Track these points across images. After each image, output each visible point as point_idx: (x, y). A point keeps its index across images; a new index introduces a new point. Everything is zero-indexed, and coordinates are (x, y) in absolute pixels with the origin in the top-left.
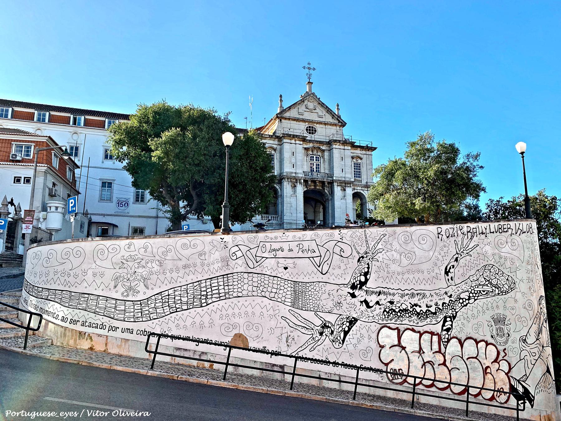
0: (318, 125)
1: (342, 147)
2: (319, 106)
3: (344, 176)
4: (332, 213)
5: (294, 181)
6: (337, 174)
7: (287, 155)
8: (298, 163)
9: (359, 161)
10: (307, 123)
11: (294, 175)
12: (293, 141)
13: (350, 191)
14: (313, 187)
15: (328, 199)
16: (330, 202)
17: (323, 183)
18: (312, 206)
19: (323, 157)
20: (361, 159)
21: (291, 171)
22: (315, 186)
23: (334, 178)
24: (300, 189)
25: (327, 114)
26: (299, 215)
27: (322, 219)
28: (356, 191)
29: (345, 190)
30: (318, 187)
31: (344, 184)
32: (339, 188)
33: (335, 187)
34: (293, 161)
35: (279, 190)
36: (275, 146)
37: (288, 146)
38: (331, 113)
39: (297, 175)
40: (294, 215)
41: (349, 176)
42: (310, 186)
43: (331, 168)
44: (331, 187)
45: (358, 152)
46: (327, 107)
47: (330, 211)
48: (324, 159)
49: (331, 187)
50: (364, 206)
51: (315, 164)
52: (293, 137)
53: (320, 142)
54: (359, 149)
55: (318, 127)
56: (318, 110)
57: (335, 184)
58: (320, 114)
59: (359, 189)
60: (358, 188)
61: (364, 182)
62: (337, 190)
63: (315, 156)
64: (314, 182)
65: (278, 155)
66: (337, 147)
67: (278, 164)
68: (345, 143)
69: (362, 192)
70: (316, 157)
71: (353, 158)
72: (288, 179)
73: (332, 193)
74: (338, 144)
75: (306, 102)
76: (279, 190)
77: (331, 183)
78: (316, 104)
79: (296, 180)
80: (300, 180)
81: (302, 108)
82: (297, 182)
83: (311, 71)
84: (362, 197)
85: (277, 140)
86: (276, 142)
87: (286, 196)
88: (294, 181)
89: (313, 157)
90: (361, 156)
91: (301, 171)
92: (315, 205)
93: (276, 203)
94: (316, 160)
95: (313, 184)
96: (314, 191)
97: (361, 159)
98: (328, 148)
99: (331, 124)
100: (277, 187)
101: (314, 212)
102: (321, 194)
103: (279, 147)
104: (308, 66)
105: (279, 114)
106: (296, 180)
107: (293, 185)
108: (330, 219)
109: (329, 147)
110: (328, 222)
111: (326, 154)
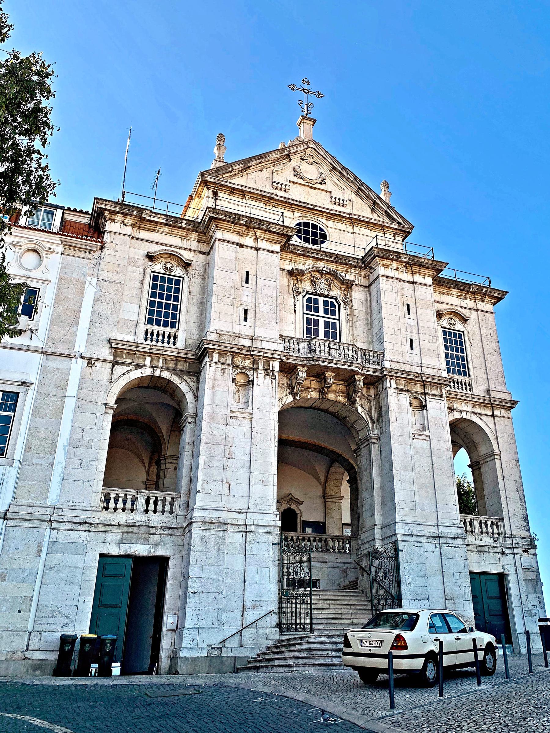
0: (330, 223)
1: (407, 277)
2: (334, 176)
3: (417, 360)
4: (382, 488)
5: (247, 362)
6: (395, 354)
7: (220, 278)
8: (263, 308)
9: (459, 326)
10: (297, 214)
11: (247, 343)
12: (248, 241)
13: (438, 411)
14: (315, 394)
15: (367, 439)
16: (375, 449)
17: (348, 378)
18: (319, 481)
19: (348, 302)
20: (465, 320)
21: (237, 329)
22: (321, 391)
23: (387, 364)
24: (269, 397)
25: (355, 199)
26: (256, 489)
27: (347, 519)
28: (457, 415)
29: (423, 407)
30: (331, 396)
31: (421, 388)
32: (405, 399)
33: (391, 392)
34: (247, 299)
35: (189, 397)
36: (187, 255)
37: (229, 254)
38: (368, 197)
39: (257, 344)
40: (239, 490)
41: (435, 363)
42: (307, 389)
43: (376, 333)
44: (377, 396)
45: (453, 300)
46: (356, 178)
47: (377, 483)
48: (351, 309)
49: (377, 396)
50: (485, 469)
51: (321, 312)
52: (249, 227)
53: (338, 256)
54: (455, 292)
55: (331, 227)
56: (329, 186)
57: (391, 385)
58: (337, 194)
59: (465, 411)
60: (463, 407)
61: (479, 390)
62: (398, 404)
63: (321, 300)
64: (317, 373)
65: (197, 281)
66: (390, 273)
67: (194, 309)
68: (414, 264)
69: (475, 419)
70: (326, 303)
71: (439, 315)
72: (222, 354)
73: (381, 415)
74: (394, 264)
75: (295, 161)
76: (189, 397)
77: (375, 382)
78: (325, 169)
79: (255, 362)
80: (268, 360)
81: (284, 174)
82: (255, 370)
83: (312, 98)
84: (477, 438)
85: (194, 236)
86: (194, 244)
87: (213, 416)
88: (248, 363)
89: (316, 301)
90: (466, 313)
91: (274, 335)
92: (328, 472)
93: (51, 324)
94: (326, 311)
95: (314, 384)
96: (319, 410)
97: (465, 320)
98: (363, 281)
99: (368, 224)
100: (184, 387)
101: (324, 497)
102: (341, 422)
103: (198, 261)
104: (305, 86)
105: (210, 172)
106: (255, 362)
107: (241, 379)
108: (377, 509)
109: (367, 277)
110: (367, 525)
111: (358, 295)
